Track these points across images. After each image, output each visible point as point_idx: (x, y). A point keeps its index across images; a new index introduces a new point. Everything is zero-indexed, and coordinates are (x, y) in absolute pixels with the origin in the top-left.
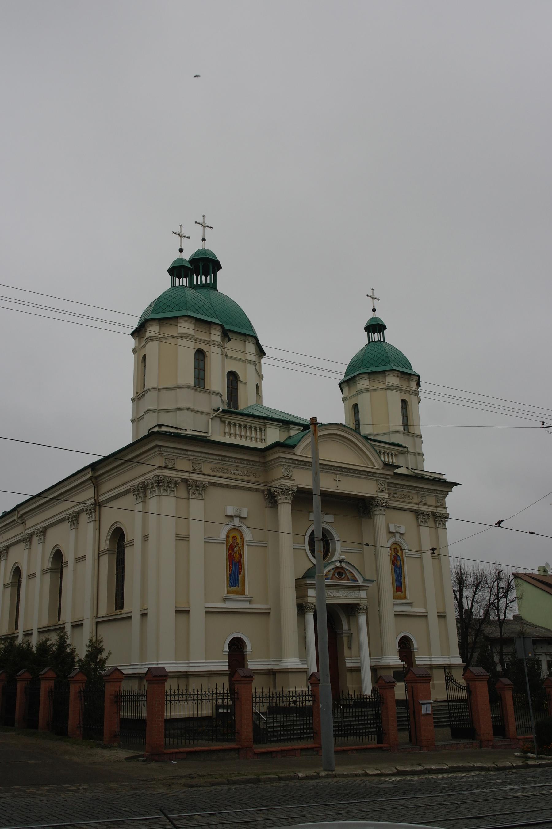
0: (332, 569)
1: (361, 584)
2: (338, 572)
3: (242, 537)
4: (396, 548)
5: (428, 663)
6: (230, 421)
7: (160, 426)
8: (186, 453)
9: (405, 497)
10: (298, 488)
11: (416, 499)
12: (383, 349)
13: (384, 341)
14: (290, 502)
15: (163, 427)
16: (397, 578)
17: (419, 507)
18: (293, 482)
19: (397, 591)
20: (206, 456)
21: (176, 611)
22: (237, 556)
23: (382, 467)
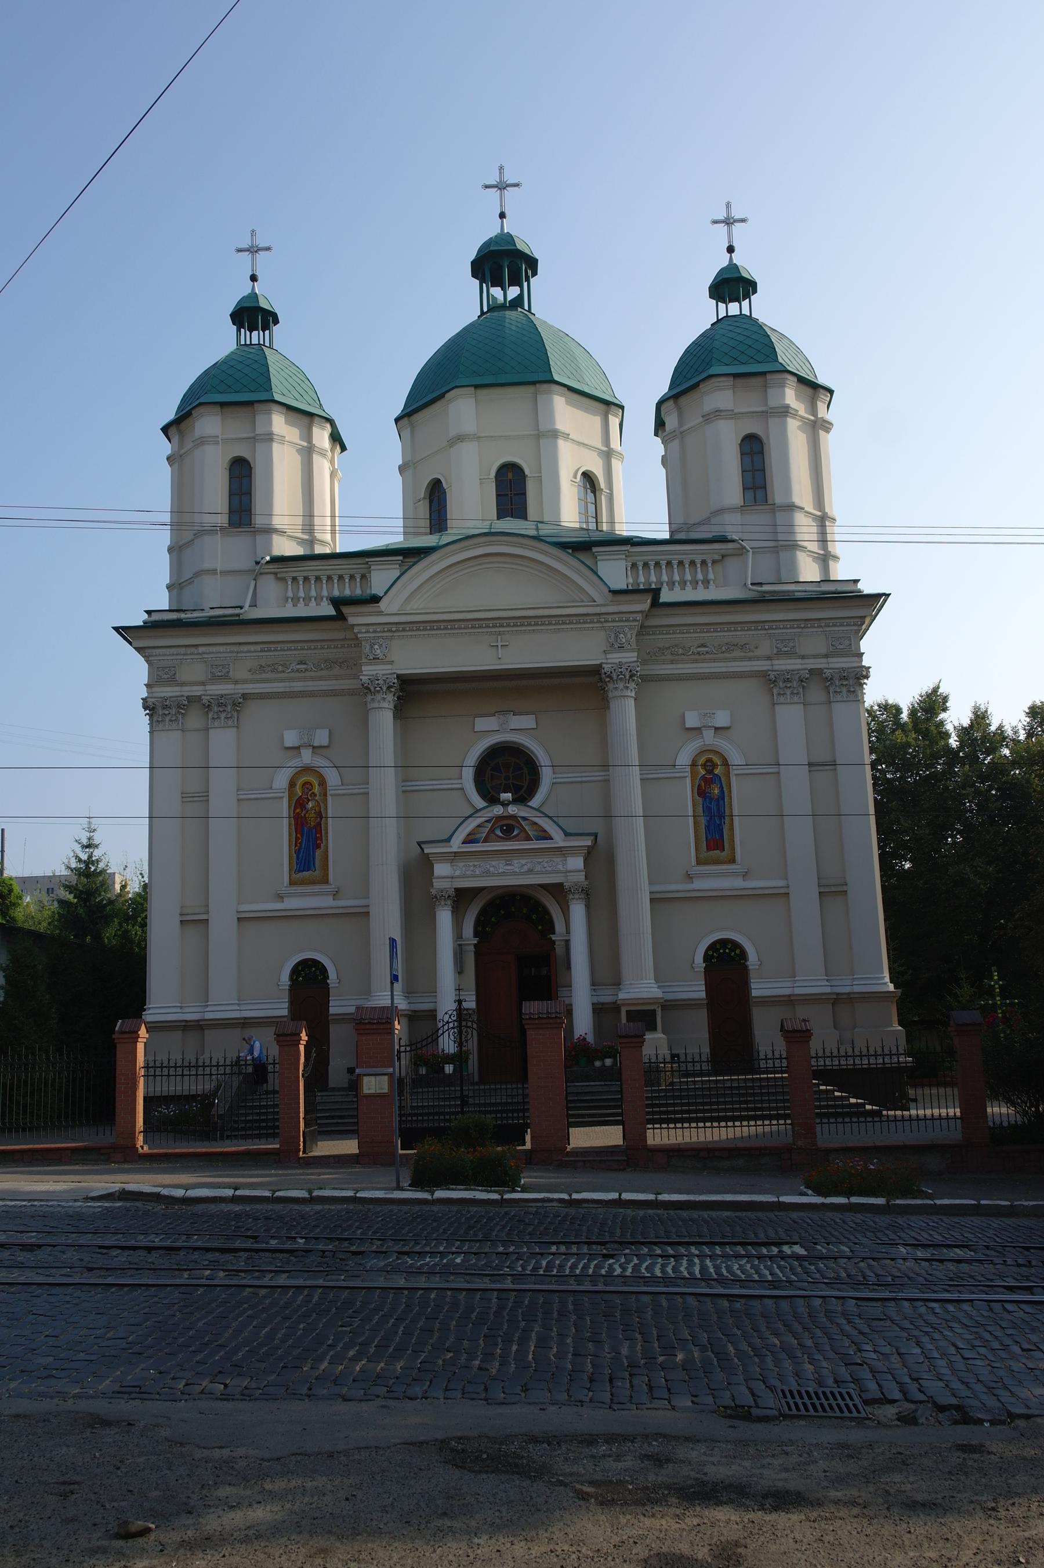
3: (323, 783)
4: (709, 760)
5: (788, 992)
6: (294, 574)
7: (149, 612)
10: (399, 677)
11: (766, 648)
14: (392, 706)
15: (764, 586)
16: (709, 822)
17: (772, 665)
18: (389, 667)
19: (709, 849)
20: (235, 648)
21: (238, 918)
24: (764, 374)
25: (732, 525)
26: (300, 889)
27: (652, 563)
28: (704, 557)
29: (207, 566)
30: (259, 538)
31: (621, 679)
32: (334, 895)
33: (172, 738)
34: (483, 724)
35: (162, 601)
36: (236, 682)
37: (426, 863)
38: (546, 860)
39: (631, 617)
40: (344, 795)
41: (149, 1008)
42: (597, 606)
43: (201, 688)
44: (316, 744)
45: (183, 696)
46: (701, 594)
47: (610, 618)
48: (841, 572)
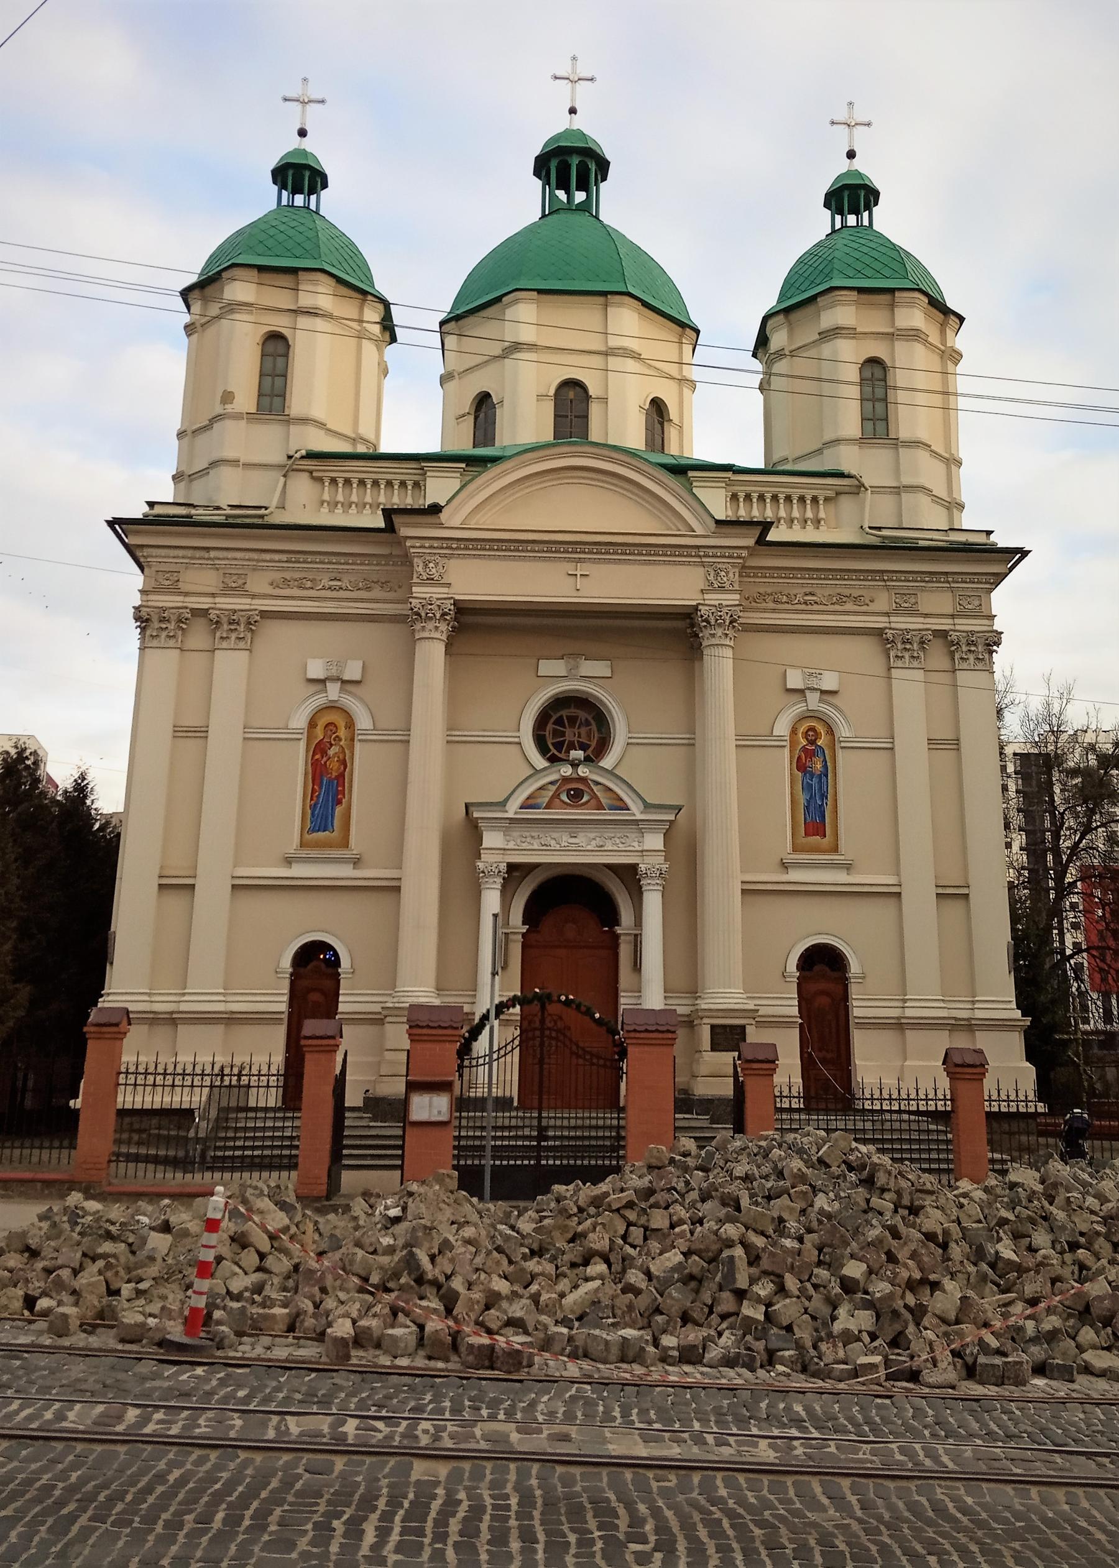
0: (552, 783)
1: (639, 817)
2: (569, 791)
3: (350, 724)
7: (151, 504)
8: (207, 555)
9: (844, 599)
10: (456, 603)
11: (883, 602)
12: (310, 234)
13: (317, 212)
14: (444, 637)
16: (808, 802)
18: (445, 590)
19: (807, 834)
20: (255, 556)
22: (334, 766)
23: (713, 530)
24: (891, 291)
25: (848, 459)
26: (314, 853)
27: (755, 495)
28: (815, 493)
29: (230, 454)
30: (294, 429)
31: (720, 625)
32: (355, 863)
33: (167, 659)
34: (548, 667)
35: (166, 492)
36: (253, 596)
37: (473, 830)
38: (618, 835)
39: (736, 552)
40: (286, 739)
41: (108, 994)
42: (697, 536)
43: (209, 600)
44: (346, 678)
45: (186, 608)
46: (810, 535)
47: (711, 552)
48: (969, 520)
